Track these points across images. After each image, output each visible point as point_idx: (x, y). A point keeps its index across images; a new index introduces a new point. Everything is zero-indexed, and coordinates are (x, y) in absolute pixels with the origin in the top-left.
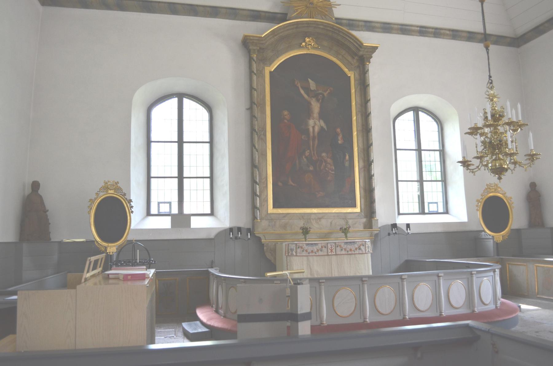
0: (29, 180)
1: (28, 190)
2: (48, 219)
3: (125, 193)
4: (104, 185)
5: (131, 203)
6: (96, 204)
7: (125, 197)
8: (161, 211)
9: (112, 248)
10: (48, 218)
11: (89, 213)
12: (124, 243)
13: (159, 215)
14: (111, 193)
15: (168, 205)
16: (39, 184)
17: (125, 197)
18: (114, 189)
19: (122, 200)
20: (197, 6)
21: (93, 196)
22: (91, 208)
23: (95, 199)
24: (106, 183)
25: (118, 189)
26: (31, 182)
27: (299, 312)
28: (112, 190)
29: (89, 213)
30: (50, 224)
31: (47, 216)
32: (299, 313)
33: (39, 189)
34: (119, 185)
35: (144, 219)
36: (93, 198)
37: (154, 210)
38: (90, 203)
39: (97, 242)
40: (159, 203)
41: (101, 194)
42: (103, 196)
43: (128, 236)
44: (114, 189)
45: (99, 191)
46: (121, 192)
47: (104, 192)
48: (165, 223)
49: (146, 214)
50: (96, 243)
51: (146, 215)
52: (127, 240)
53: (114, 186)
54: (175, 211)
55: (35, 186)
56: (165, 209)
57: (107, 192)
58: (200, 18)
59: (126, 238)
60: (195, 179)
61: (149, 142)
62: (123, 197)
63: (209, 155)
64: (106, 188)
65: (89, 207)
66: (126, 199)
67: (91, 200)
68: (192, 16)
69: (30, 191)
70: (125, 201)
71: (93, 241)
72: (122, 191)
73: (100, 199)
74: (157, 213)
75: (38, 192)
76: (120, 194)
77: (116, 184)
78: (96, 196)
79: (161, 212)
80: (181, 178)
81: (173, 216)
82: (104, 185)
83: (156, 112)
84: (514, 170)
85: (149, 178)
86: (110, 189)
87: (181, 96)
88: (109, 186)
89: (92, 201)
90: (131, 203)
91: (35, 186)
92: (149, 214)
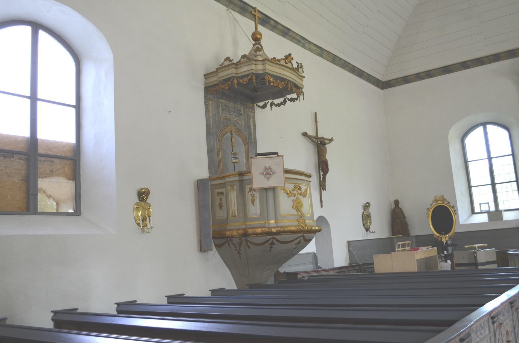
0: (393, 200)
1: (393, 206)
2: (407, 222)
3: (449, 202)
4: (434, 199)
5: (454, 208)
6: (432, 211)
7: (450, 204)
8: (482, 210)
9: (445, 239)
10: (407, 221)
11: (428, 217)
12: (452, 234)
13: (482, 212)
14: (440, 203)
15: (487, 205)
16: (399, 201)
17: (450, 204)
18: (441, 200)
19: (448, 206)
20: (482, 58)
21: (429, 207)
22: (428, 214)
23: (430, 208)
24: (436, 197)
25: (444, 200)
26: (394, 201)
27: (478, 262)
28: (440, 201)
29: (427, 217)
30: (408, 225)
31: (406, 220)
32: (478, 262)
33: (399, 204)
34: (444, 197)
35: (470, 216)
36: (429, 208)
37: (477, 210)
38: (427, 211)
39: (435, 235)
40: (480, 204)
41: (434, 204)
42: (435, 205)
43: (456, 229)
44: (441, 200)
45: (432, 203)
46: (446, 202)
47: (435, 203)
48: (483, 218)
49: (471, 212)
50: (434, 235)
51: (471, 213)
52: (455, 232)
53: (441, 198)
54: (493, 209)
55: (397, 202)
56: (485, 208)
57: (437, 202)
58: (487, 65)
59: (453, 231)
60: (510, 183)
61: (466, 162)
62: (448, 205)
63: (470, 178)
64: (436, 200)
65: (427, 213)
66: (450, 205)
67: (427, 209)
68: (481, 65)
69: (394, 206)
70: (450, 207)
71: (433, 235)
72: (447, 201)
73: (433, 208)
74: (479, 211)
75: (399, 206)
76: (446, 203)
77: (442, 197)
78: (430, 207)
79: (483, 211)
80: (493, 184)
81: (489, 213)
82: (434, 199)
83: (469, 140)
84: (241, 250)
85: (470, 187)
86: (439, 201)
87: (484, 124)
88: (438, 199)
89: (428, 210)
90: (454, 208)
91: (397, 202)
92: (473, 212)
